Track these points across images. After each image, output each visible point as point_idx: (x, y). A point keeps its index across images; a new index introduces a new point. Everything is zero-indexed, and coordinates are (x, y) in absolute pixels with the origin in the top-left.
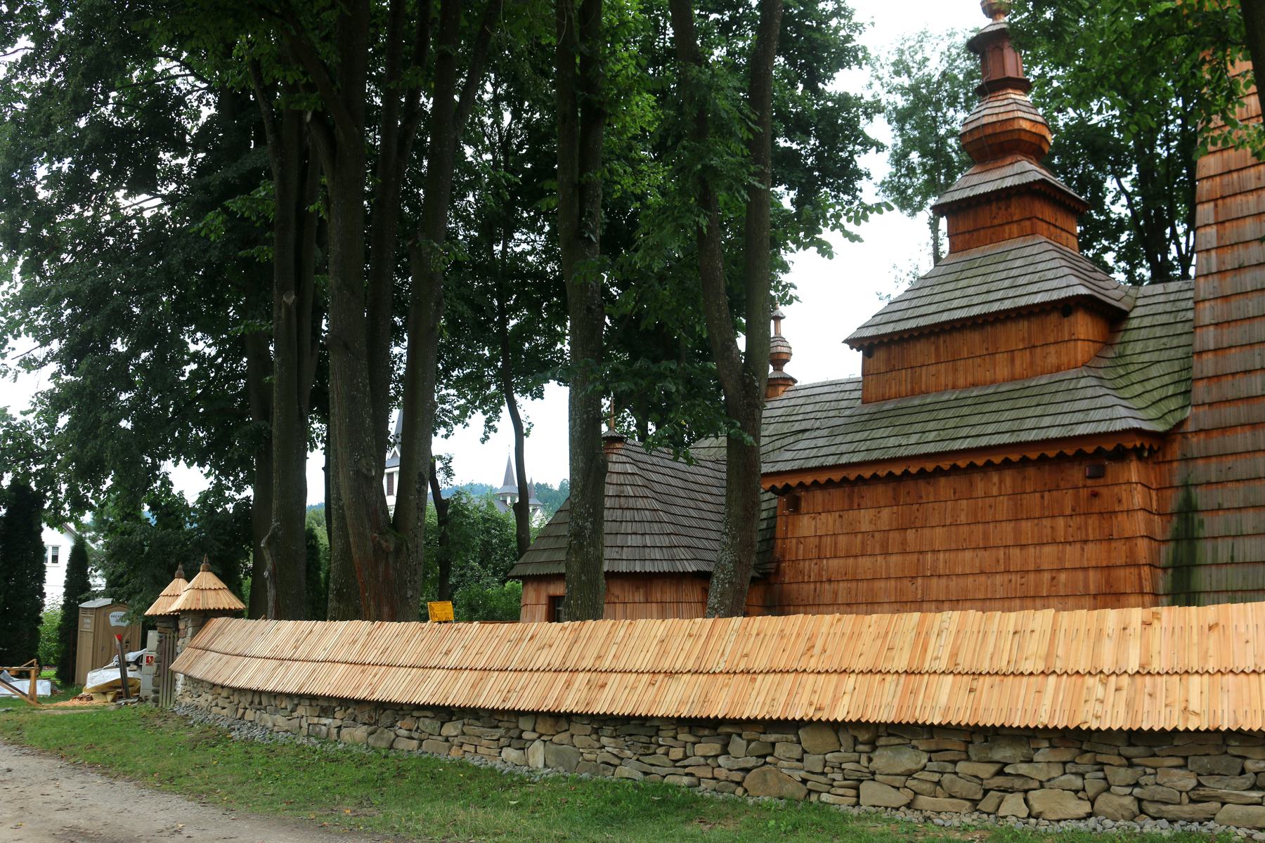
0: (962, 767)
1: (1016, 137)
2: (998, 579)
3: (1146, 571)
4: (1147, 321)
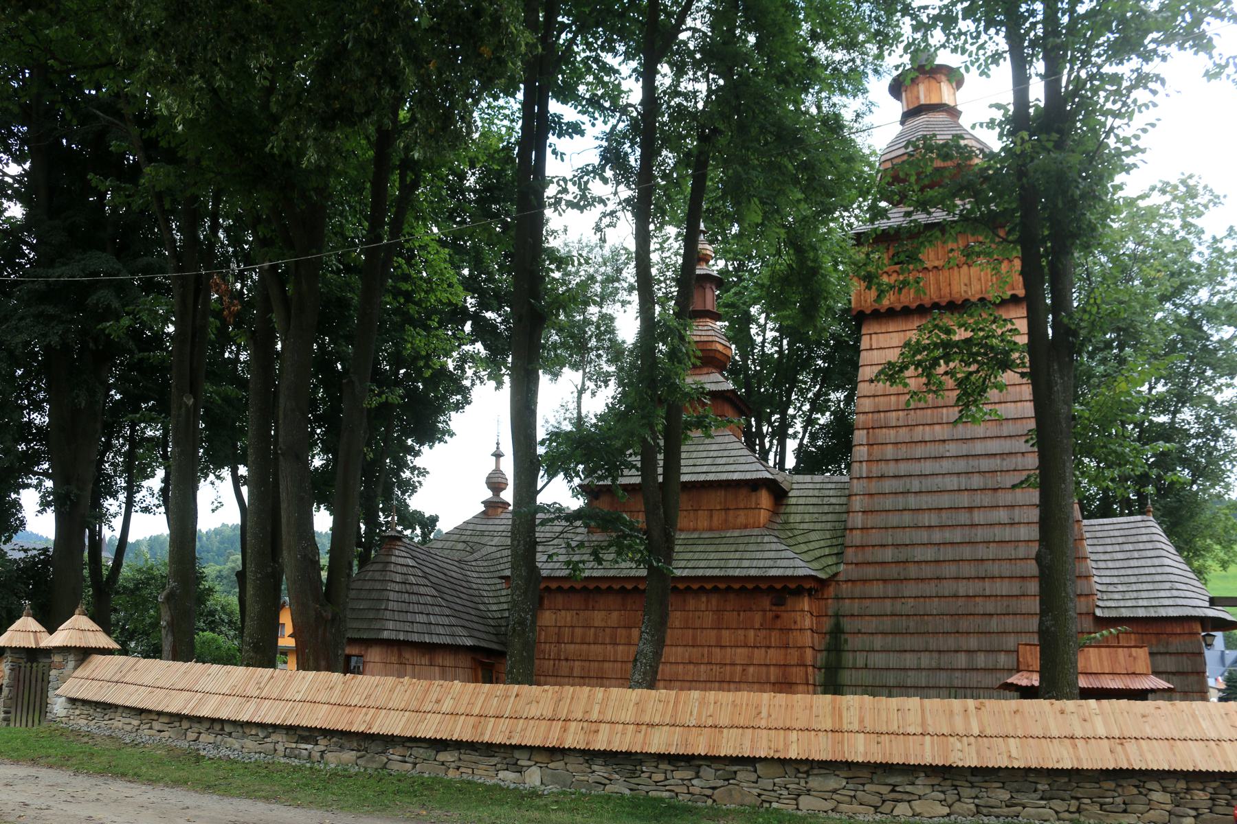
0: (867, 787)
1: (712, 354)
2: (703, 668)
3: (810, 669)
4: (802, 501)
